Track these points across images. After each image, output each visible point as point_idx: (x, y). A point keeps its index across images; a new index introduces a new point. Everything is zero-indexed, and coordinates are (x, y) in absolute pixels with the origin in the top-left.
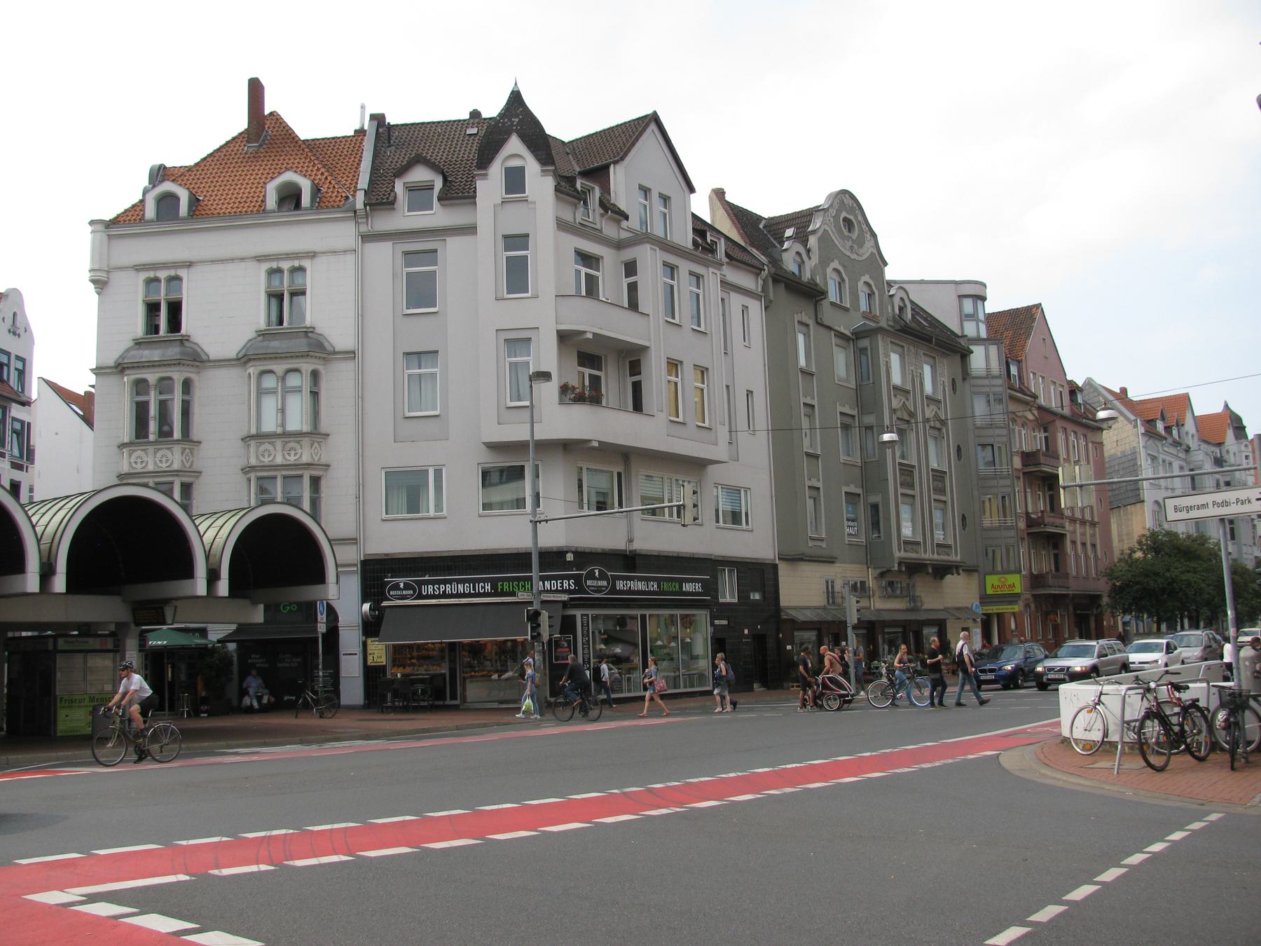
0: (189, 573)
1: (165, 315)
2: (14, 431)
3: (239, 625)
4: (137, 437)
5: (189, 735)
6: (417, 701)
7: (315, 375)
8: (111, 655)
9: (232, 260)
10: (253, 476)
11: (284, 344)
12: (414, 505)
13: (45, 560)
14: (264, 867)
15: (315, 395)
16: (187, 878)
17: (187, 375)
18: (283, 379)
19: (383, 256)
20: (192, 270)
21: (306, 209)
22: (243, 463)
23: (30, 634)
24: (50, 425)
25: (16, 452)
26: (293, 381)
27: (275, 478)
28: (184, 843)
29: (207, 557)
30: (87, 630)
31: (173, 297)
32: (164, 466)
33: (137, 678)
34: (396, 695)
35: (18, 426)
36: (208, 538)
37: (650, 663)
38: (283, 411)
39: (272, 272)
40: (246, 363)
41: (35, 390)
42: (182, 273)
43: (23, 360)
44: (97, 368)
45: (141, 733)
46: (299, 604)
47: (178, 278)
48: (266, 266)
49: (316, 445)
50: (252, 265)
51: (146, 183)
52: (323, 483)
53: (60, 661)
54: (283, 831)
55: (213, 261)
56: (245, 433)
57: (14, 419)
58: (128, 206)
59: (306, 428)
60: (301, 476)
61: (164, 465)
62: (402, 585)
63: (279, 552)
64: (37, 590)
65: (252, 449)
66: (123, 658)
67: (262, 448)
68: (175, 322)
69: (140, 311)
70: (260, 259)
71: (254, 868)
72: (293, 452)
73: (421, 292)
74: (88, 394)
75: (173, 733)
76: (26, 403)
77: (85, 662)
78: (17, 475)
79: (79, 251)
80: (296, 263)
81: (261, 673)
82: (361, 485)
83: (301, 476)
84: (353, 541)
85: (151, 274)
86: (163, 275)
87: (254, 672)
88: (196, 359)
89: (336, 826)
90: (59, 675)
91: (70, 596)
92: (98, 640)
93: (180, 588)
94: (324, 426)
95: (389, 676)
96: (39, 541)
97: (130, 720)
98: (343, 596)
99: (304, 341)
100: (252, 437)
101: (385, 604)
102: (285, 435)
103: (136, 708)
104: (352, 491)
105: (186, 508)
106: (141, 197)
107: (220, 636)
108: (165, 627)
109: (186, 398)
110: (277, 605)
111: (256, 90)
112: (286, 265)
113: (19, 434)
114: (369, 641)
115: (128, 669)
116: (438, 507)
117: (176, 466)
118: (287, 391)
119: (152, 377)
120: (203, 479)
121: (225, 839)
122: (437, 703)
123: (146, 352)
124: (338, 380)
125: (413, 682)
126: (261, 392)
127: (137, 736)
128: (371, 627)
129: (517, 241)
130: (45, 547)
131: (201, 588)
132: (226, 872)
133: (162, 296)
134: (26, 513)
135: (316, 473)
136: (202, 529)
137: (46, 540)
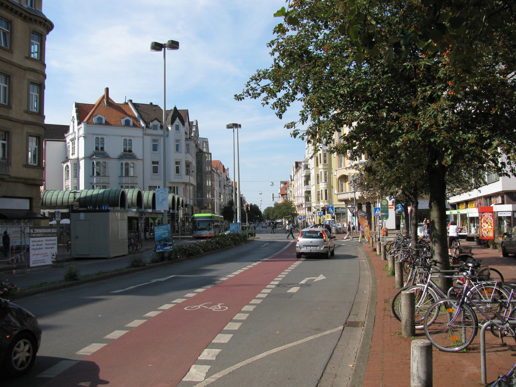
111: (107, 89)
129: (178, 141)
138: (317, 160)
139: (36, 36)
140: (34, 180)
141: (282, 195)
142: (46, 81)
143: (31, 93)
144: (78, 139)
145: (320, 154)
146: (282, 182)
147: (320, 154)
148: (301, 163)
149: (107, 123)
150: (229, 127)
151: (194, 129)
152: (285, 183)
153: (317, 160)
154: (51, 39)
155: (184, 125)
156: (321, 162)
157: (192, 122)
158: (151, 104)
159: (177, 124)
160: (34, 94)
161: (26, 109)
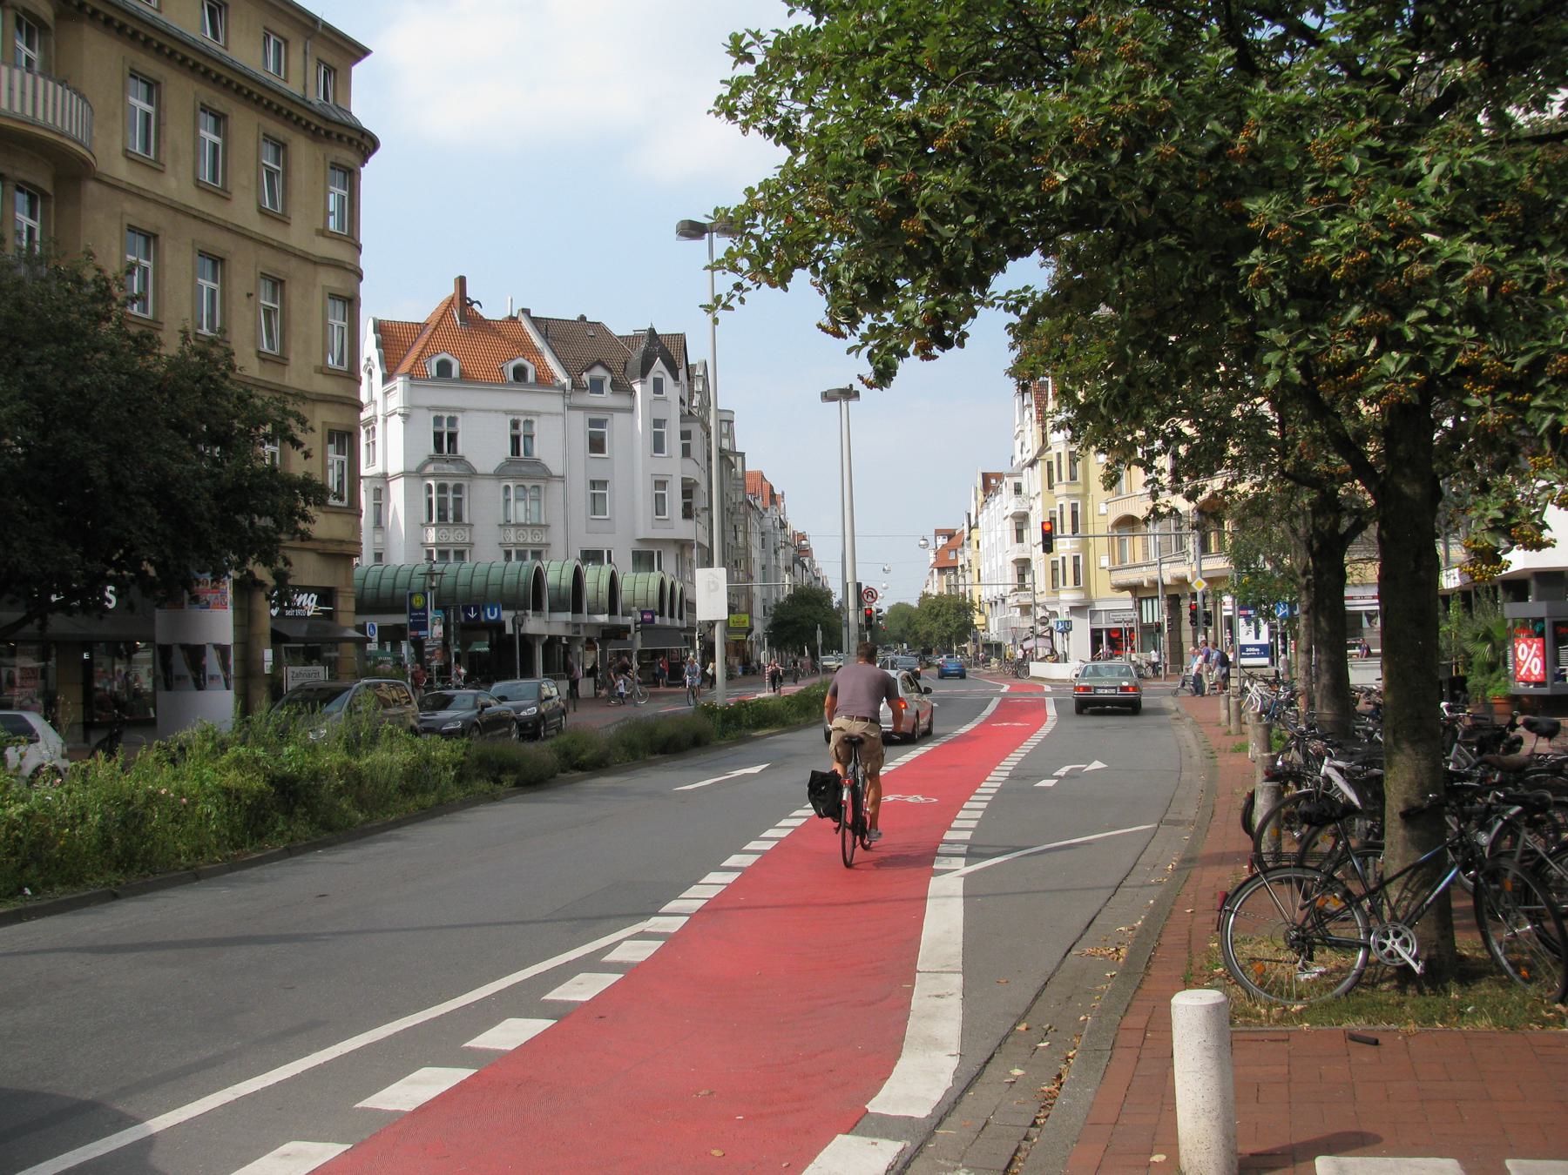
1: (445, 442)
31: (452, 430)
37: (1189, 648)
70: (507, 412)
88: (472, 474)
111: (462, 281)
112: (522, 419)
119: (451, 483)
129: (658, 423)
138: (1050, 470)
139: (339, 175)
140: (341, 542)
141: (942, 570)
142: (362, 284)
143: (331, 320)
144: (385, 421)
145: (1059, 455)
146: (938, 533)
147: (1059, 455)
148: (999, 477)
149: (464, 377)
150: (828, 396)
151: (699, 387)
152: (950, 535)
153: (1050, 470)
154: (370, 173)
155: (676, 377)
156: (1060, 479)
157: (694, 366)
158: (583, 318)
159: (659, 376)
160: (337, 322)
161: (320, 364)
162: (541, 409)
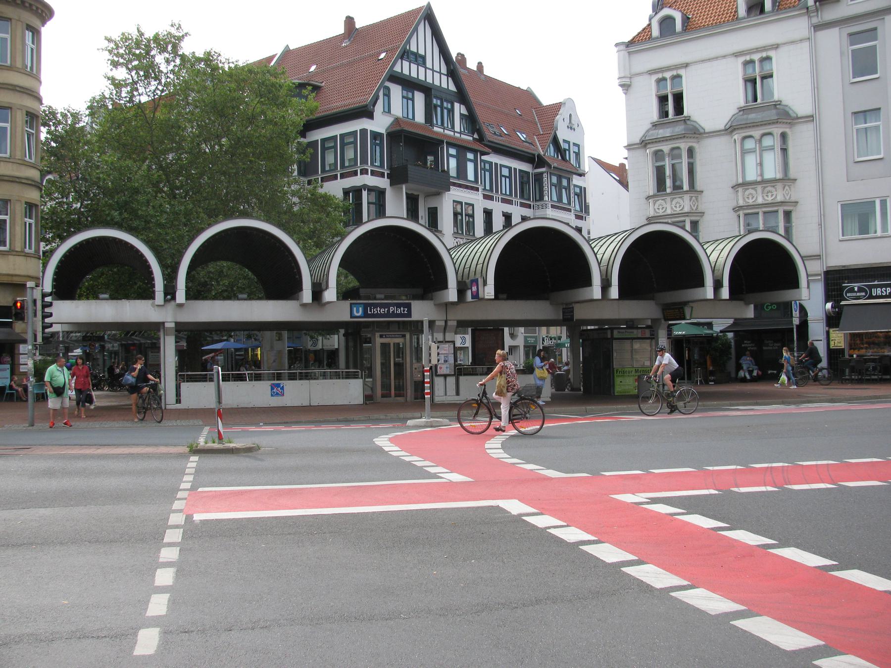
0: (701, 283)
1: (672, 103)
2: (576, 194)
3: (736, 319)
4: (658, 191)
5: (704, 396)
6: (870, 375)
7: (784, 136)
8: (648, 341)
9: (716, 58)
10: (741, 213)
11: (762, 115)
12: (864, 228)
13: (604, 277)
14: (770, 489)
15: (784, 151)
16: (716, 492)
17: (690, 144)
18: (760, 141)
19: (832, 39)
20: (689, 69)
21: (769, 12)
22: (734, 204)
23: (593, 327)
24: (597, 186)
25: (578, 208)
26: (767, 142)
27: (758, 213)
28: (711, 468)
29: (713, 271)
30: (631, 324)
31: (677, 90)
32: (678, 210)
33: (667, 356)
34: (853, 370)
35: (578, 190)
36: (713, 258)
38: (761, 164)
39: (746, 64)
40: (732, 132)
41: (587, 165)
42: (682, 72)
43: (578, 146)
44: (629, 145)
45: (670, 395)
46: (779, 304)
47: (679, 76)
48: (742, 59)
49: (787, 187)
50: (732, 60)
51: (650, 11)
52: (793, 215)
53: (616, 345)
54: (781, 464)
55: (703, 61)
56: (734, 183)
57: (575, 186)
58: (640, 29)
59: (779, 176)
60: (777, 211)
61: (678, 209)
62: (856, 289)
63: (764, 266)
64: (456, 300)
65: (740, 194)
66: (657, 343)
67: (747, 192)
68: (679, 109)
69: (654, 103)
70: (737, 55)
71: (763, 489)
72: (770, 194)
73: (864, 64)
74: (622, 166)
75: (693, 394)
76: (581, 175)
77: (632, 346)
78: (579, 223)
79: (610, 65)
80: (764, 55)
81: (754, 355)
82: (822, 216)
83: (777, 211)
84: (818, 257)
85: (660, 76)
86: (668, 75)
87: (748, 353)
88: (696, 133)
89: (819, 463)
90: (615, 354)
91: (621, 302)
92: (640, 331)
93: (695, 294)
94: (792, 174)
95: (847, 356)
96: (599, 264)
97: (664, 385)
98: (812, 298)
99: (774, 111)
100: (739, 185)
101: (843, 303)
102: (764, 182)
103: (667, 377)
104: (816, 220)
105: (696, 238)
106: (648, 23)
107: (722, 328)
108: (683, 322)
109: (691, 161)
110: (762, 305)
112: (756, 57)
113: (578, 195)
114: (831, 330)
115: (662, 350)
116: (885, 228)
117: (686, 209)
118: (763, 150)
119: (666, 148)
120: (706, 218)
121: (739, 467)
122: (885, 377)
123: (661, 131)
124: (802, 140)
125: (866, 361)
126: (744, 152)
127: (668, 395)
128: (833, 321)
130: (604, 269)
131: (709, 293)
132: (743, 490)
133: (669, 90)
134: (590, 245)
135: (788, 208)
136: (709, 251)
137: (604, 263)
150: (106, 38)
162: (779, 41)
